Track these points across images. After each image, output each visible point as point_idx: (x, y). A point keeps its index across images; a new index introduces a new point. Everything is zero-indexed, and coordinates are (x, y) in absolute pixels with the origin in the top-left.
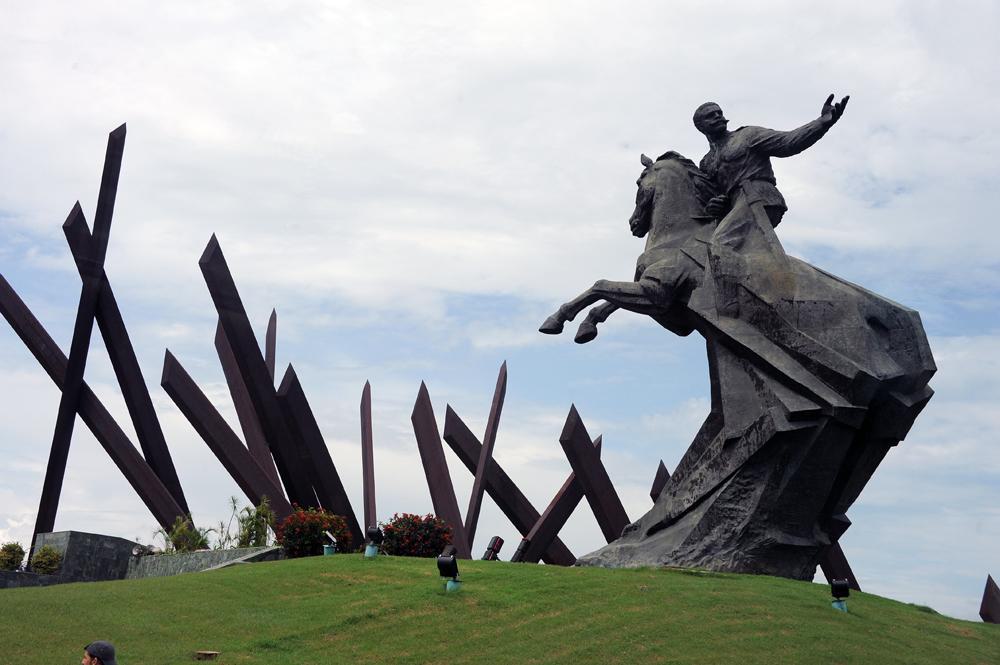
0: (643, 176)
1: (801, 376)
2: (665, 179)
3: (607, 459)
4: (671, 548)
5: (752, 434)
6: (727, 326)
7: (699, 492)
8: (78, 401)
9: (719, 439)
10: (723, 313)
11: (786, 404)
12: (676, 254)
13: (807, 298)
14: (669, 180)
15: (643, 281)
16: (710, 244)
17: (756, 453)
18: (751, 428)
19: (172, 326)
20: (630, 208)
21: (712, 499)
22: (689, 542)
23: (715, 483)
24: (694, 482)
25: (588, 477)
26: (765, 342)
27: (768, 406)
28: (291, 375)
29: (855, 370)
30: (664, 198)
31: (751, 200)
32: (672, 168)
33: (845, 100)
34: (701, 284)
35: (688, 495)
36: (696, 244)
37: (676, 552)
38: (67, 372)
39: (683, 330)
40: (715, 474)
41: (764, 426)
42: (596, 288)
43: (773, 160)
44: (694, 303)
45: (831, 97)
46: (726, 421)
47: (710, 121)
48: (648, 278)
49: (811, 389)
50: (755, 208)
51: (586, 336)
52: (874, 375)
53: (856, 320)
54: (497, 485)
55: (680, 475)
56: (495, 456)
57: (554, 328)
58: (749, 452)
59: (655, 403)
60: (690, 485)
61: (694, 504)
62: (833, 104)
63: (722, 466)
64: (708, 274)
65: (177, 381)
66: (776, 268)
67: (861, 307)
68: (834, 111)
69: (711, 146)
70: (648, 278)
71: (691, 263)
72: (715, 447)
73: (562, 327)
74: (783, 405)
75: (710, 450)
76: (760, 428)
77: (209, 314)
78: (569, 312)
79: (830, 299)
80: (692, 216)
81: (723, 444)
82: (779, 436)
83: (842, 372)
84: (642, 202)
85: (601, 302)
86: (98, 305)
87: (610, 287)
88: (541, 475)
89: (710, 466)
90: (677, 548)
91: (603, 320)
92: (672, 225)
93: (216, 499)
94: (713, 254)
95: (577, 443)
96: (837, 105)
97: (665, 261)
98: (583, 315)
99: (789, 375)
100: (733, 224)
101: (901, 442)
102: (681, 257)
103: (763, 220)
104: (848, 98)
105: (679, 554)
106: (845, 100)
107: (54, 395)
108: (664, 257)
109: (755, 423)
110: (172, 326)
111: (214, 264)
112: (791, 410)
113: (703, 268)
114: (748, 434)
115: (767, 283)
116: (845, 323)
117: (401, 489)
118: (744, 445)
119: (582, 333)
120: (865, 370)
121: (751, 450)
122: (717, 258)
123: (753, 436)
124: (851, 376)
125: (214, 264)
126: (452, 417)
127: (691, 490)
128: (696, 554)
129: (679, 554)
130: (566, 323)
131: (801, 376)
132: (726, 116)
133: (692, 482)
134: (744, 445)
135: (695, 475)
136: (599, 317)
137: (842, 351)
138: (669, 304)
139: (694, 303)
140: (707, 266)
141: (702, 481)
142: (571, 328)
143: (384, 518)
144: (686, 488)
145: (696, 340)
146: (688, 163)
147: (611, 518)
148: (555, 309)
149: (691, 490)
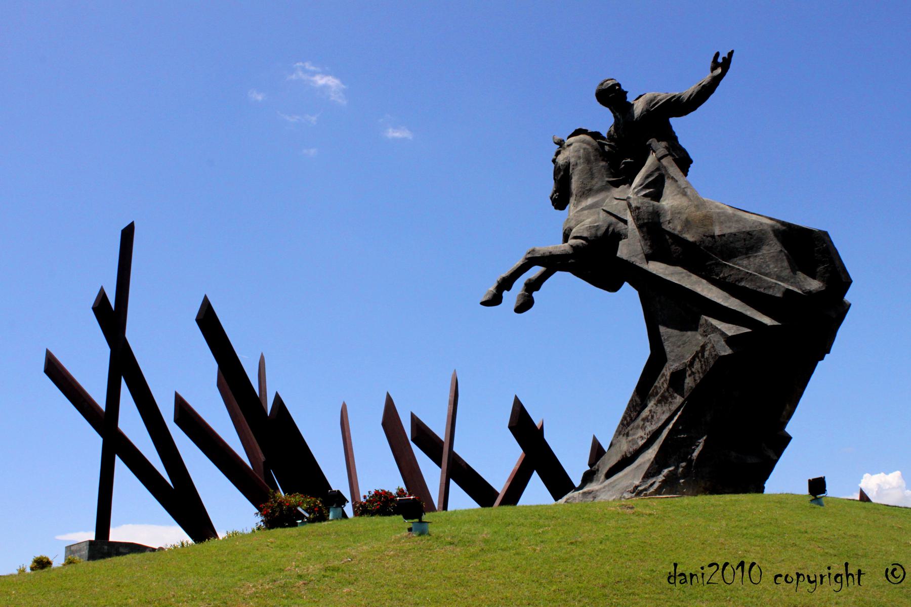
0: (558, 153)
1: (733, 304)
2: (578, 151)
3: (549, 437)
4: (631, 484)
5: (696, 363)
6: (656, 268)
7: (651, 427)
8: (116, 446)
9: (664, 375)
10: (649, 258)
11: (723, 330)
12: (599, 214)
13: (727, 231)
14: (582, 151)
15: (572, 242)
16: (629, 198)
17: (702, 380)
18: (694, 359)
19: (181, 372)
20: (549, 186)
21: (665, 433)
22: (648, 475)
23: (664, 417)
24: (645, 419)
25: (538, 457)
26: (694, 277)
27: (706, 336)
28: (278, 400)
29: (783, 289)
30: (579, 168)
31: (659, 156)
32: (583, 142)
33: (731, 54)
34: (626, 236)
35: (641, 433)
36: (616, 202)
37: (636, 487)
38: (104, 421)
39: (613, 287)
40: (664, 409)
41: (706, 354)
42: (529, 256)
43: (673, 121)
44: (624, 251)
45: (717, 55)
46: (668, 356)
47: (612, 96)
48: (575, 238)
49: (744, 312)
50: (665, 162)
51: (525, 305)
52: (800, 292)
53: (773, 248)
54: (461, 474)
55: (628, 419)
56: (456, 449)
57: (495, 300)
58: (695, 380)
59: (589, 364)
60: (641, 423)
61: (648, 439)
62: (720, 60)
63: (670, 399)
64: (632, 225)
65: (187, 417)
66: (693, 209)
67: (777, 233)
68: (722, 64)
69: (615, 117)
70: (575, 238)
71: (614, 220)
72: (662, 383)
73: (501, 298)
74: (720, 330)
75: (656, 387)
76: (703, 356)
77: (211, 366)
78: (506, 284)
79: (748, 229)
80: (607, 179)
81: (668, 378)
82: (721, 360)
83: (770, 292)
84: (559, 176)
85: (535, 271)
86: (124, 366)
87: (541, 252)
88: (497, 460)
89: (659, 402)
90: (637, 483)
91: (538, 289)
92: (590, 190)
93: (230, 509)
94: (633, 205)
95: (523, 427)
96: (724, 58)
97: (590, 220)
98: (519, 286)
99: (722, 303)
100: (647, 177)
101: (827, 355)
102: (603, 215)
103: (674, 170)
104: (733, 51)
105: (640, 488)
106: (731, 54)
107: (97, 441)
108: (588, 218)
109: (697, 353)
110: (181, 372)
111: (208, 321)
112: (730, 334)
113: (625, 222)
114: (691, 363)
115: (687, 224)
116: (765, 250)
117: (381, 474)
118: (690, 376)
119: (520, 302)
120: (791, 288)
121: (697, 378)
122: (638, 208)
123: (697, 365)
124: (779, 295)
125: (208, 321)
126: (417, 424)
127: (643, 428)
128: (656, 486)
129: (640, 488)
130: (505, 294)
131: (733, 304)
132: (624, 88)
133: (643, 420)
134: (690, 376)
135: (645, 413)
136: (533, 286)
137: (766, 275)
138: (596, 261)
139: (624, 251)
140: (629, 218)
141: (652, 417)
142: (511, 297)
143: (366, 489)
144: (638, 427)
145: (628, 295)
146: (596, 135)
147: (559, 484)
148: (492, 288)
149: (643, 428)
